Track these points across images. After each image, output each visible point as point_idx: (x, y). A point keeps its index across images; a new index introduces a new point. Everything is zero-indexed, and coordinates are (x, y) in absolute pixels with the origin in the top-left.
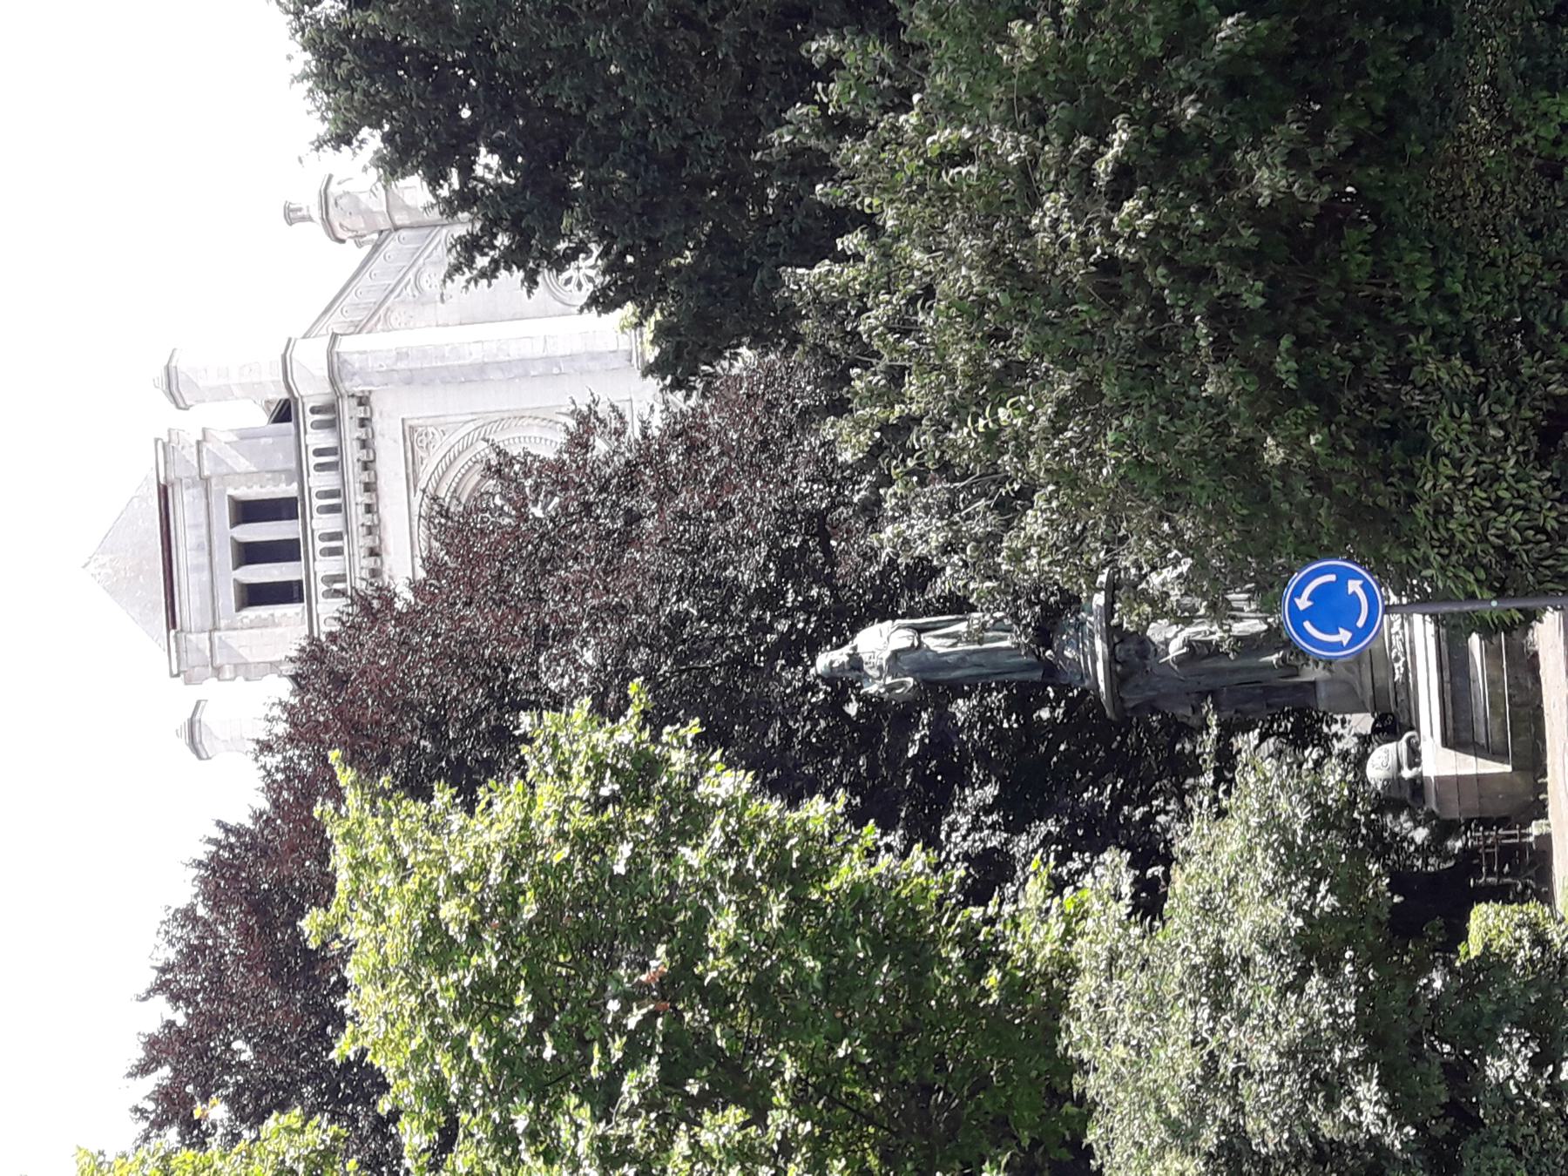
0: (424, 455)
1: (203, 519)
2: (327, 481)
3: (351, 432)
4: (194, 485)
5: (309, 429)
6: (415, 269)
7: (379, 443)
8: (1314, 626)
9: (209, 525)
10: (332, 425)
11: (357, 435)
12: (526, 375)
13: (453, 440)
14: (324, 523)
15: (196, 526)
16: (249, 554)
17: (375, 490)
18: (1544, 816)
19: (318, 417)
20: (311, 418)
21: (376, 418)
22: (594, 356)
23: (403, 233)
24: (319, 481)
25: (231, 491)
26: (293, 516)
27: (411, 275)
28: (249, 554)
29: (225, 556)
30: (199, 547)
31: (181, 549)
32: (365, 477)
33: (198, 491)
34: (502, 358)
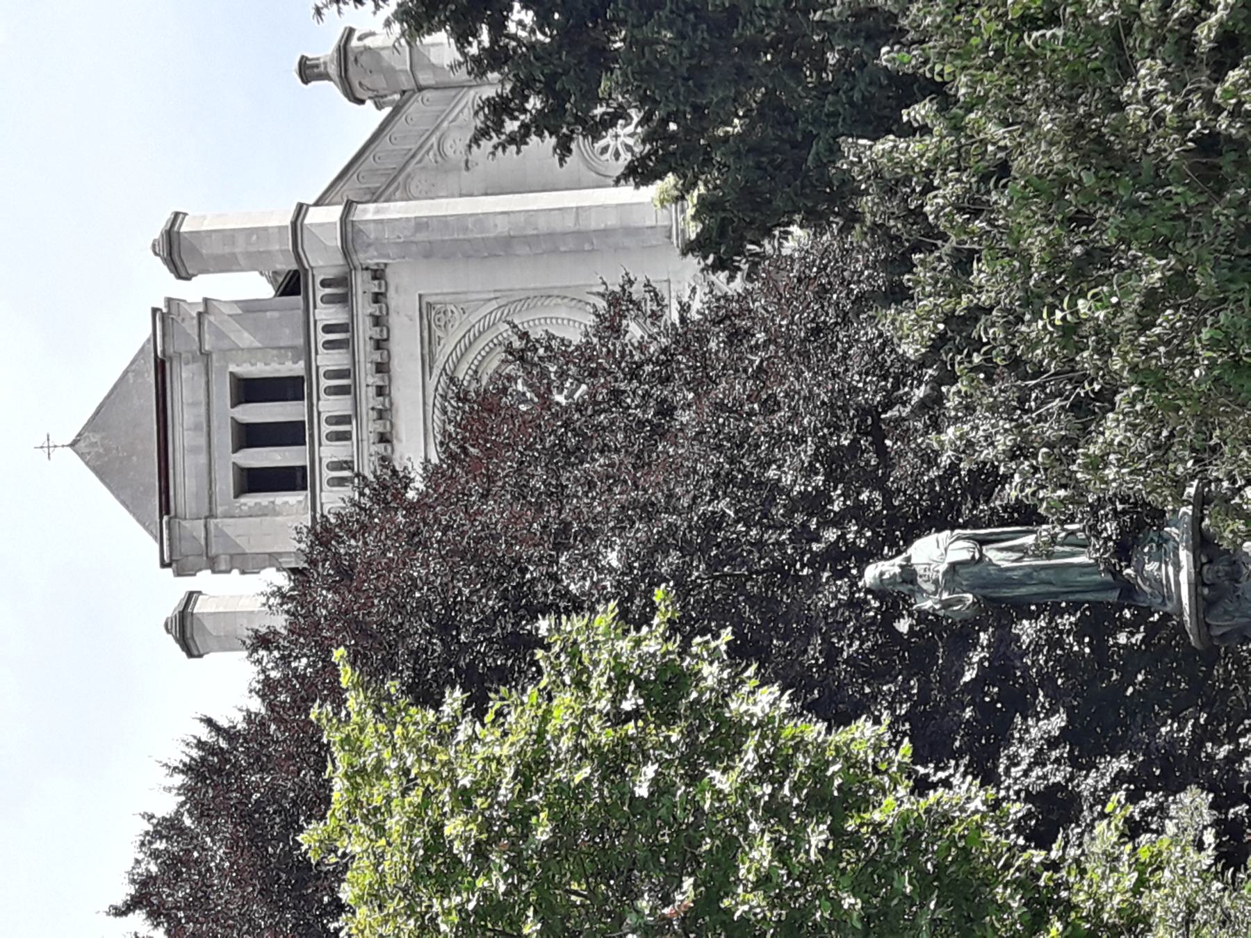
0: (439, 333)
3: (364, 308)
5: (324, 440)
6: (438, 134)
10: (344, 299)
11: (370, 311)
12: (555, 251)
14: (331, 406)
16: (249, 436)
17: (388, 371)
19: (328, 291)
20: (322, 292)
21: (391, 293)
23: (427, 94)
24: (328, 360)
25: (233, 368)
26: (347, 331)
27: (434, 140)
28: (249, 436)
29: (224, 437)
30: (197, 428)
31: (178, 428)
32: (377, 357)
33: (197, 367)
34: (530, 232)
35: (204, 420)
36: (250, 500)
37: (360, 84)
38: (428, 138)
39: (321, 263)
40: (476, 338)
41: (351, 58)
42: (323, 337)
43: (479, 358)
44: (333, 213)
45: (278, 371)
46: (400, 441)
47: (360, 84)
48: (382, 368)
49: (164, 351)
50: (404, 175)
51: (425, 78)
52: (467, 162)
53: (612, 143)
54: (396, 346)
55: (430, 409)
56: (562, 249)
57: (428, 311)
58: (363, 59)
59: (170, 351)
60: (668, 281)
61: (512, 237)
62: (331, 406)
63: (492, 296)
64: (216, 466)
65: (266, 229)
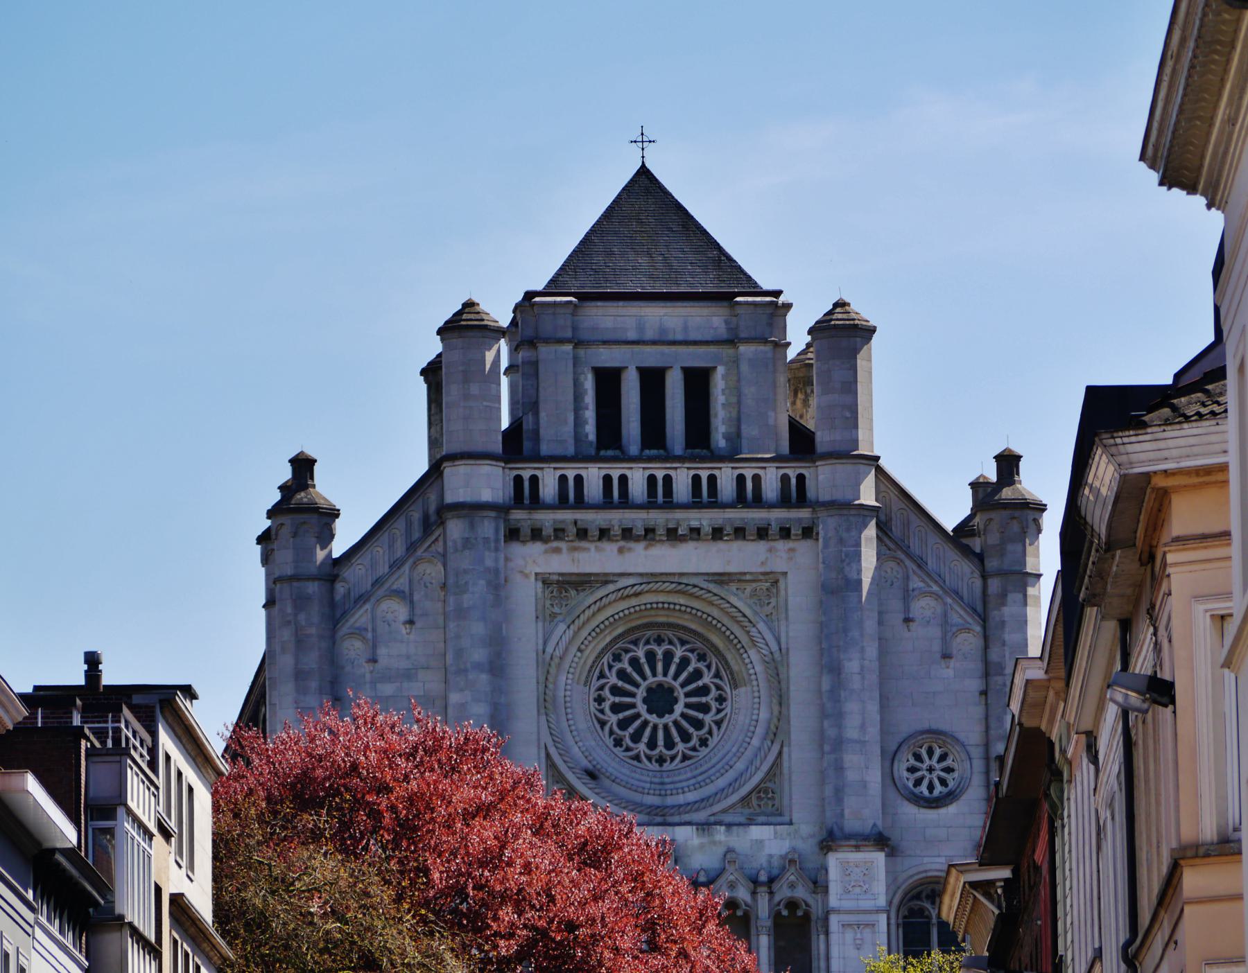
1: (693, 336)
3: (777, 516)
4: (729, 329)
5: (782, 472)
8: (571, 302)
9: (539, 733)
10: (784, 501)
12: (823, 715)
13: (761, 626)
16: (652, 380)
17: (737, 538)
19: (793, 481)
20: (793, 474)
21: (790, 544)
23: (978, 583)
24: (726, 477)
25: (720, 370)
27: (935, 588)
28: (652, 380)
29: (652, 357)
30: (663, 330)
32: (774, 528)
33: (722, 332)
35: (671, 337)
36: (589, 383)
37: (282, 524)
38: (936, 582)
39: (821, 478)
41: (1017, 513)
42: (571, 475)
44: (868, 496)
46: (646, 548)
47: (282, 524)
48: (717, 534)
50: (902, 556)
51: (994, 585)
53: (924, 766)
54: (610, 548)
56: (826, 723)
58: (1015, 527)
61: (839, 674)
62: (637, 478)
63: (783, 646)
65: (856, 427)
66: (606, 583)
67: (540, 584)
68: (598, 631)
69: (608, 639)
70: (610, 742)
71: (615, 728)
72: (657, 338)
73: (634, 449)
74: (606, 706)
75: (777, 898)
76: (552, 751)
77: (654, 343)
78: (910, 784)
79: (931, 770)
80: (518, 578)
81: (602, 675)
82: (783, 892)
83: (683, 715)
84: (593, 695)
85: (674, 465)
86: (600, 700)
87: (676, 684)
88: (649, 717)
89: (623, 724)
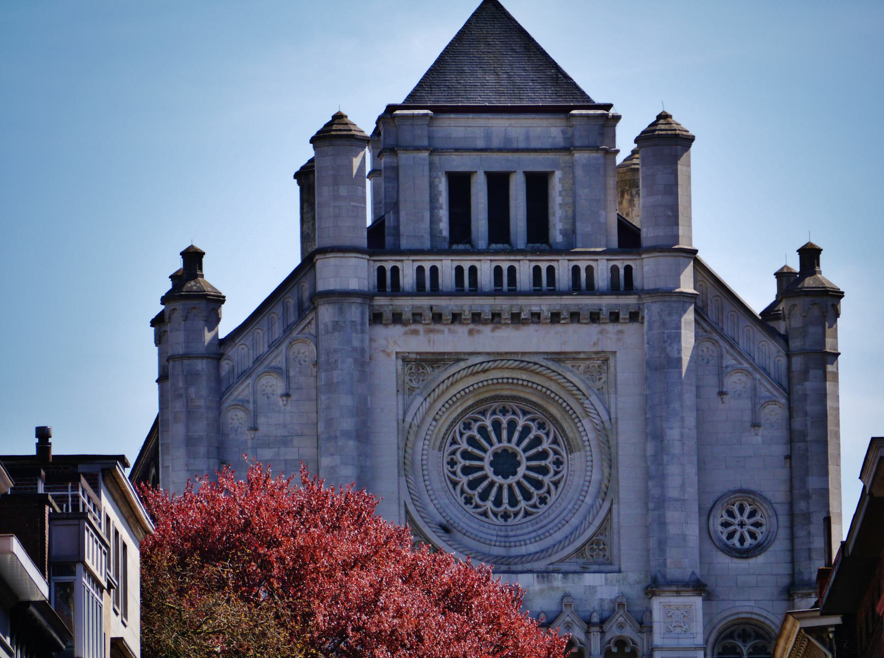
0: (582, 368)
1: (535, 144)
2: (408, 278)
3: (607, 302)
6: (751, 369)
7: (594, 328)
10: (614, 289)
11: (604, 309)
14: (524, 270)
15: (527, 138)
17: (572, 322)
18: (75, 575)
19: (622, 272)
20: (621, 266)
22: (662, 545)
23: (783, 361)
24: (563, 268)
25: (558, 174)
29: (498, 163)
30: (507, 139)
33: (560, 141)
34: (665, 458)
35: (515, 146)
36: (443, 186)
38: (746, 360)
39: (646, 269)
40: (577, 399)
43: (560, 401)
45: (554, 215)
46: (493, 330)
49: (574, 115)
50: (717, 338)
52: (411, 423)
53: (736, 522)
54: (461, 330)
55: (519, 358)
56: (650, 484)
57: (604, 358)
59: (574, 122)
60: (620, 571)
61: (662, 441)
63: (613, 416)
64: (474, 156)
66: (458, 360)
67: (400, 362)
68: (451, 403)
69: (460, 410)
70: (461, 500)
71: (466, 488)
72: (502, 146)
73: (482, 244)
74: (458, 468)
75: (608, 637)
76: (411, 508)
77: (500, 150)
78: (724, 537)
79: (742, 525)
80: (381, 357)
81: (454, 442)
82: (613, 632)
83: (525, 477)
84: (447, 458)
85: (518, 258)
86: (452, 463)
87: (519, 450)
88: (495, 478)
89: (473, 485)
